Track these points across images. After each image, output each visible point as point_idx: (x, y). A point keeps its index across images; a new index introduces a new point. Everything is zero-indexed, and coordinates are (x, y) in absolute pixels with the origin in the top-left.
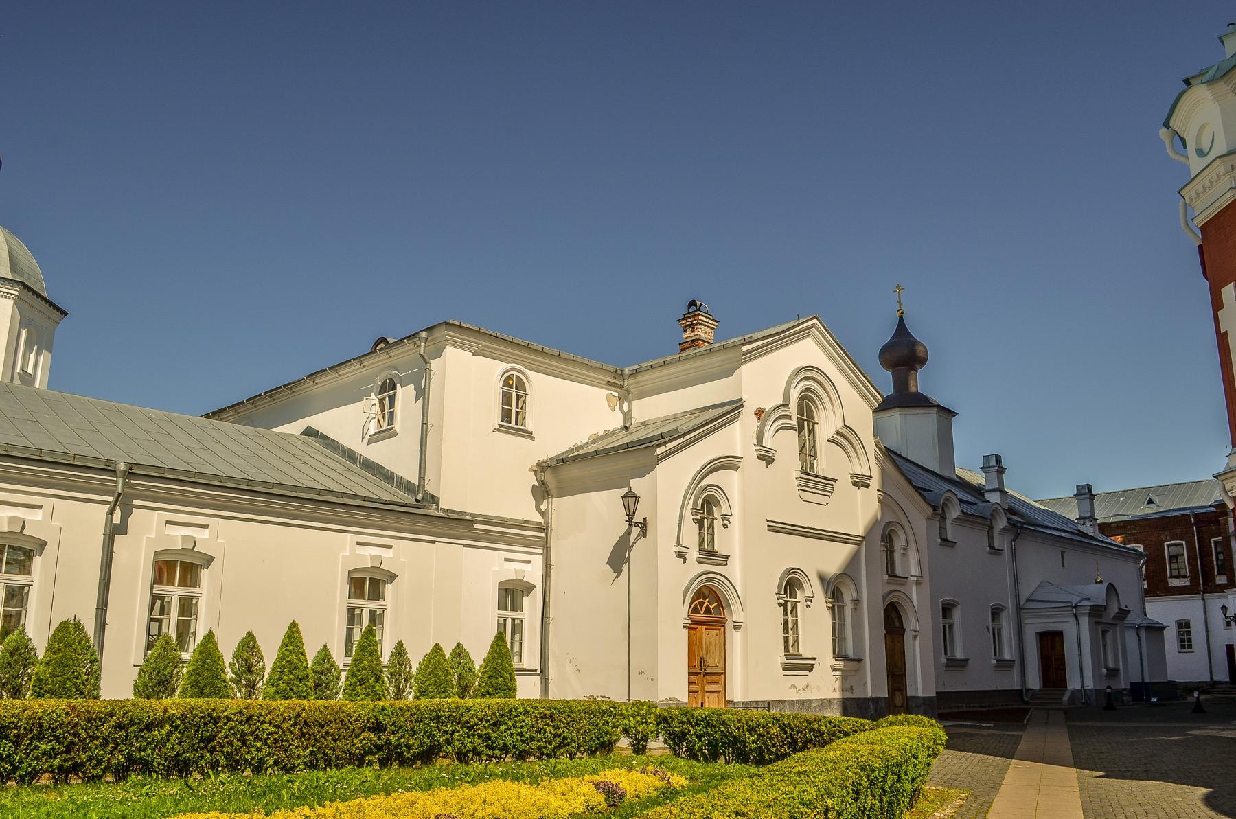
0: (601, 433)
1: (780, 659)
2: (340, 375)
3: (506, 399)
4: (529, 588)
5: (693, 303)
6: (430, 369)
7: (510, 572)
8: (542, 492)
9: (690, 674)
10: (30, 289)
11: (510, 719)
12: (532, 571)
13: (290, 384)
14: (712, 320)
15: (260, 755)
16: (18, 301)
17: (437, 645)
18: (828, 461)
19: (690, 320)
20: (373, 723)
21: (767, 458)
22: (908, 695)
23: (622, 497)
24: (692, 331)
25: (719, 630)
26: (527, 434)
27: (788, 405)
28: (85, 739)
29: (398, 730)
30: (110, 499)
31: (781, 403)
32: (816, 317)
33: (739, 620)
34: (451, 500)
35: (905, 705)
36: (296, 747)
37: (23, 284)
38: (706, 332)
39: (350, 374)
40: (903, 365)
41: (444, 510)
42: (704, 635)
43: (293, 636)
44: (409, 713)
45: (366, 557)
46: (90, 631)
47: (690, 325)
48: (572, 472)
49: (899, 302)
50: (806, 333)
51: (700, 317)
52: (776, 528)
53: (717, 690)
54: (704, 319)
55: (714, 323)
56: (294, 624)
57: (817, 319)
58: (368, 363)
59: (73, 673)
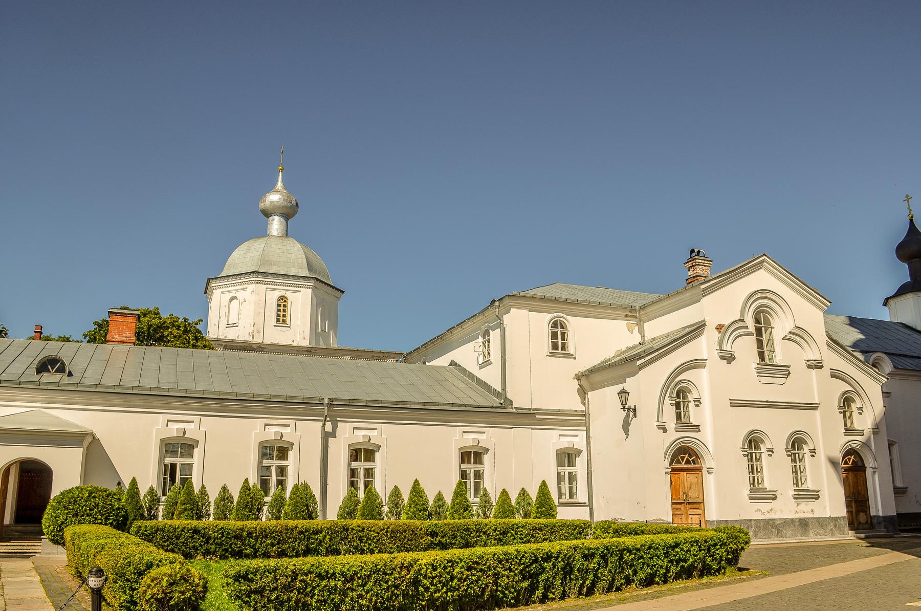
0: (624, 349)
1: (746, 492)
2: (463, 329)
3: (554, 335)
4: (579, 452)
5: (692, 251)
6: (503, 324)
7: (565, 443)
8: (582, 392)
9: (673, 503)
10: (320, 281)
11: (513, 530)
12: (579, 441)
13: (432, 340)
14: (707, 261)
15: (371, 547)
16: (314, 288)
17: (504, 490)
18: (781, 354)
19: (691, 263)
20: (430, 532)
21: (729, 358)
22: (871, 515)
23: (618, 393)
24: (694, 270)
25: (698, 474)
26: (570, 356)
27: (743, 319)
28: (285, 539)
29: (445, 535)
30: (323, 418)
31: (739, 318)
32: (764, 255)
33: (711, 467)
34: (520, 399)
35: (869, 521)
36: (389, 543)
37: (316, 278)
38: (703, 270)
39: (468, 326)
40: (915, 258)
41: (516, 408)
42: (685, 478)
43: (416, 489)
44: (450, 526)
45: (469, 440)
46: (316, 490)
47: (691, 267)
48: (596, 378)
49: (909, 208)
50: (759, 266)
51: (697, 261)
52: (735, 404)
53: (698, 513)
54: (700, 261)
55: (709, 262)
56: (416, 481)
57: (766, 256)
58: (476, 321)
59: (301, 509)
